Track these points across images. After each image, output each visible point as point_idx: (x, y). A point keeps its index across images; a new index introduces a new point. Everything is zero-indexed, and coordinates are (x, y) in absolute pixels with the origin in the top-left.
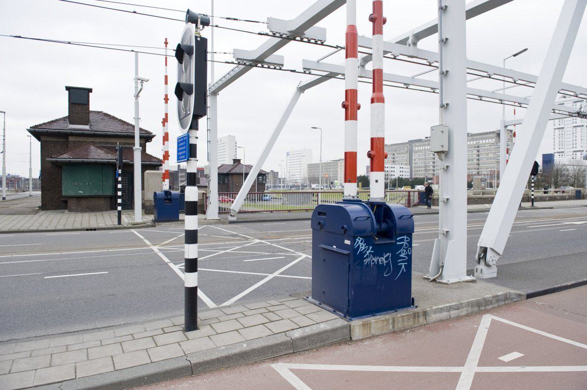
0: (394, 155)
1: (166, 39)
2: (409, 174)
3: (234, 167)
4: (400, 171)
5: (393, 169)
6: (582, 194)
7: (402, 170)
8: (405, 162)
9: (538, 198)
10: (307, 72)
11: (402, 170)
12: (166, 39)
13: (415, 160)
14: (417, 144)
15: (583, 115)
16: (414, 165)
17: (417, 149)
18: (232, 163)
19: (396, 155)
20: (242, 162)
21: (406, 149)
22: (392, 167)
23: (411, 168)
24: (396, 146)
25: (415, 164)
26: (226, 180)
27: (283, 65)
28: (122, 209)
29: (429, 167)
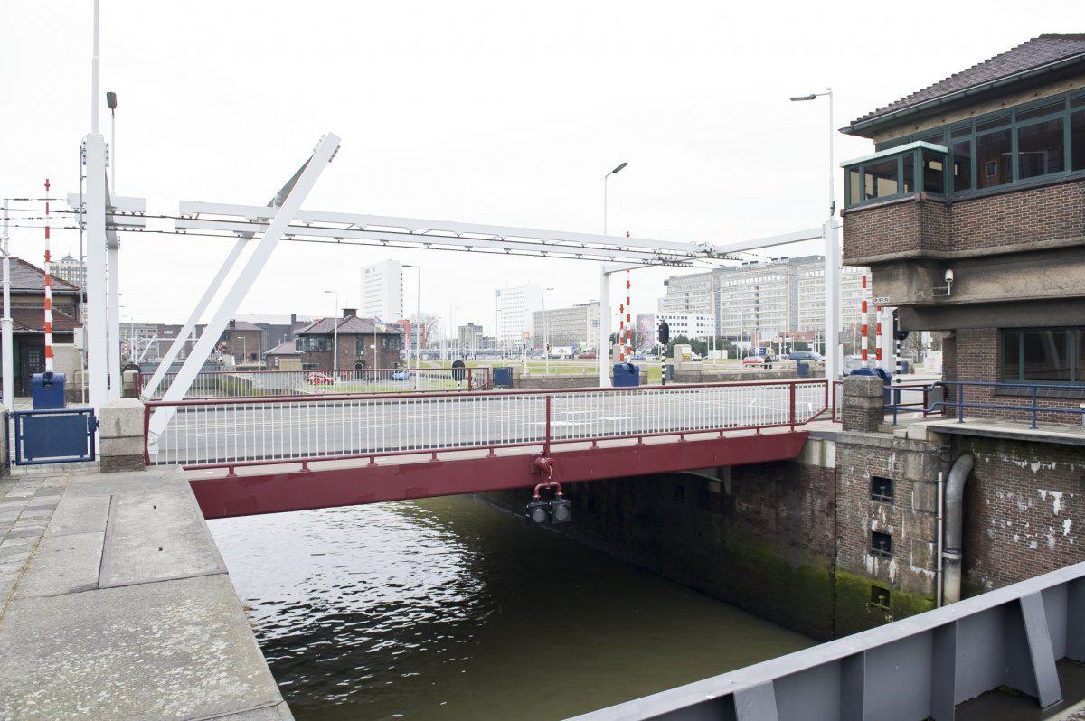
0: (688, 295)
1: (47, 180)
2: (714, 329)
3: (342, 322)
4: (686, 325)
5: (684, 321)
6: (810, 370)
7: (700, 322)
8: (708, 308)
9: (719, 377)
10: (181, 231)
11: (700, 322)
12: (47, 180)
13: (724, 304)
14: (728, 275)
15: (719, 254)
16: (722, 313)
17: (727, 283)
18: (341, 315)
19: (691, 296)
20: (359, 314)
21: (708, 284)
22: (682, 318)
23: (718, 318)
24: (698, 279)
25: (803, 305)
26: (329, 344)
27: (144, 226)
28: (36, 405)
29: (749, 316)
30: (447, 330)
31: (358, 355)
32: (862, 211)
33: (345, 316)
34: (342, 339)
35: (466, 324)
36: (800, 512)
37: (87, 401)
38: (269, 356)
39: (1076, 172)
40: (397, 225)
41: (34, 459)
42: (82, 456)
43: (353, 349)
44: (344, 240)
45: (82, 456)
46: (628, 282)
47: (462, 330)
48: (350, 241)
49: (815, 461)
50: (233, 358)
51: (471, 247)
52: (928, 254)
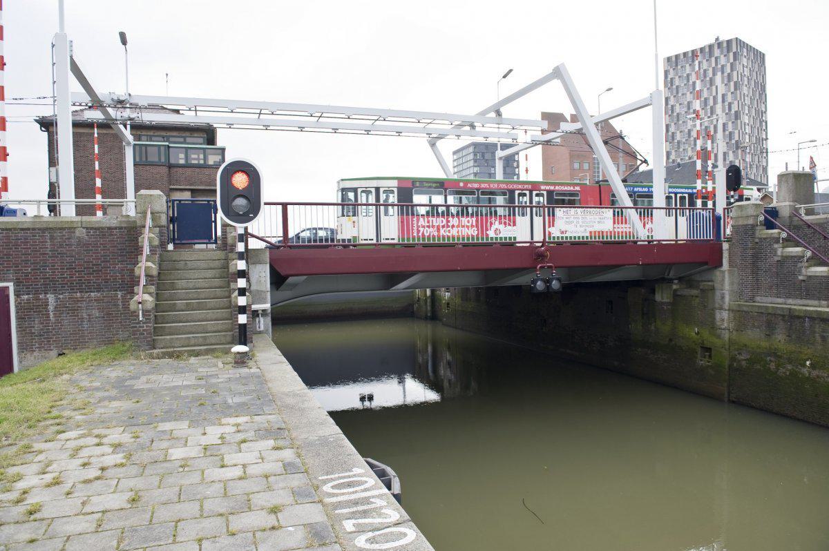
32: (216, 332)
35: (712, 41)
37: (59, 198)
39: (103, 200)
40: (244, 123)
41: (213, 220)
42: (209, 241)
44: (339, 131)
45: (209, 241)
46: (612, 89)
48: (238, 126)
49: (816, 191)
51: (269, 126)
52: (178, 133)
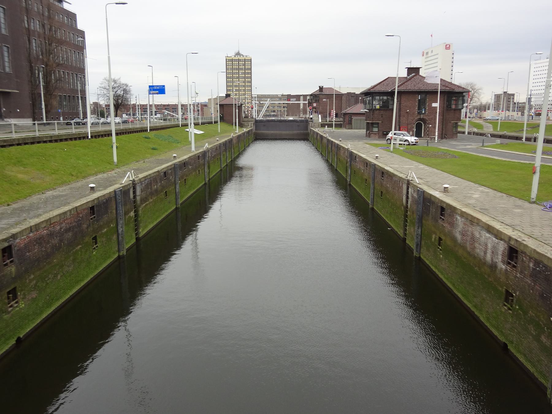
30: (481, 101)
31: (420, 113)
33: (408, 75)
34: (404, 98)
36: (429, 125)
38: (345, 114)
43: (488, 319)
47: (498, 97)
50: (320, 116)
